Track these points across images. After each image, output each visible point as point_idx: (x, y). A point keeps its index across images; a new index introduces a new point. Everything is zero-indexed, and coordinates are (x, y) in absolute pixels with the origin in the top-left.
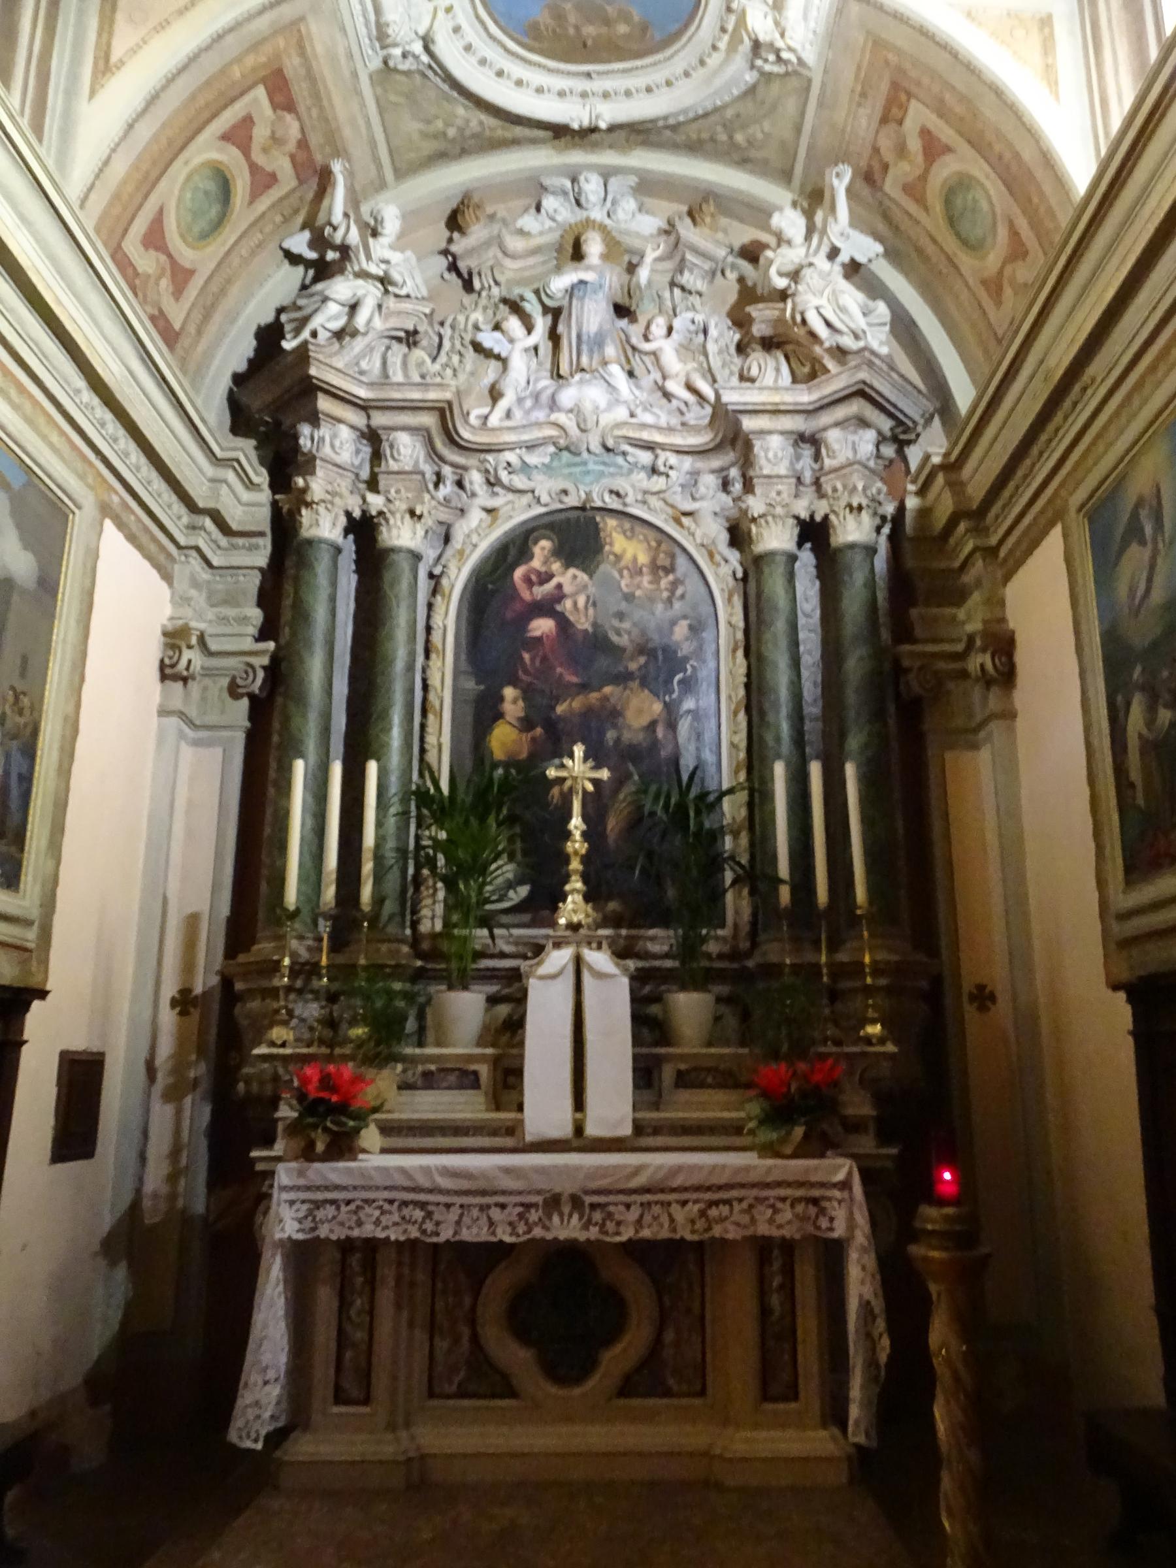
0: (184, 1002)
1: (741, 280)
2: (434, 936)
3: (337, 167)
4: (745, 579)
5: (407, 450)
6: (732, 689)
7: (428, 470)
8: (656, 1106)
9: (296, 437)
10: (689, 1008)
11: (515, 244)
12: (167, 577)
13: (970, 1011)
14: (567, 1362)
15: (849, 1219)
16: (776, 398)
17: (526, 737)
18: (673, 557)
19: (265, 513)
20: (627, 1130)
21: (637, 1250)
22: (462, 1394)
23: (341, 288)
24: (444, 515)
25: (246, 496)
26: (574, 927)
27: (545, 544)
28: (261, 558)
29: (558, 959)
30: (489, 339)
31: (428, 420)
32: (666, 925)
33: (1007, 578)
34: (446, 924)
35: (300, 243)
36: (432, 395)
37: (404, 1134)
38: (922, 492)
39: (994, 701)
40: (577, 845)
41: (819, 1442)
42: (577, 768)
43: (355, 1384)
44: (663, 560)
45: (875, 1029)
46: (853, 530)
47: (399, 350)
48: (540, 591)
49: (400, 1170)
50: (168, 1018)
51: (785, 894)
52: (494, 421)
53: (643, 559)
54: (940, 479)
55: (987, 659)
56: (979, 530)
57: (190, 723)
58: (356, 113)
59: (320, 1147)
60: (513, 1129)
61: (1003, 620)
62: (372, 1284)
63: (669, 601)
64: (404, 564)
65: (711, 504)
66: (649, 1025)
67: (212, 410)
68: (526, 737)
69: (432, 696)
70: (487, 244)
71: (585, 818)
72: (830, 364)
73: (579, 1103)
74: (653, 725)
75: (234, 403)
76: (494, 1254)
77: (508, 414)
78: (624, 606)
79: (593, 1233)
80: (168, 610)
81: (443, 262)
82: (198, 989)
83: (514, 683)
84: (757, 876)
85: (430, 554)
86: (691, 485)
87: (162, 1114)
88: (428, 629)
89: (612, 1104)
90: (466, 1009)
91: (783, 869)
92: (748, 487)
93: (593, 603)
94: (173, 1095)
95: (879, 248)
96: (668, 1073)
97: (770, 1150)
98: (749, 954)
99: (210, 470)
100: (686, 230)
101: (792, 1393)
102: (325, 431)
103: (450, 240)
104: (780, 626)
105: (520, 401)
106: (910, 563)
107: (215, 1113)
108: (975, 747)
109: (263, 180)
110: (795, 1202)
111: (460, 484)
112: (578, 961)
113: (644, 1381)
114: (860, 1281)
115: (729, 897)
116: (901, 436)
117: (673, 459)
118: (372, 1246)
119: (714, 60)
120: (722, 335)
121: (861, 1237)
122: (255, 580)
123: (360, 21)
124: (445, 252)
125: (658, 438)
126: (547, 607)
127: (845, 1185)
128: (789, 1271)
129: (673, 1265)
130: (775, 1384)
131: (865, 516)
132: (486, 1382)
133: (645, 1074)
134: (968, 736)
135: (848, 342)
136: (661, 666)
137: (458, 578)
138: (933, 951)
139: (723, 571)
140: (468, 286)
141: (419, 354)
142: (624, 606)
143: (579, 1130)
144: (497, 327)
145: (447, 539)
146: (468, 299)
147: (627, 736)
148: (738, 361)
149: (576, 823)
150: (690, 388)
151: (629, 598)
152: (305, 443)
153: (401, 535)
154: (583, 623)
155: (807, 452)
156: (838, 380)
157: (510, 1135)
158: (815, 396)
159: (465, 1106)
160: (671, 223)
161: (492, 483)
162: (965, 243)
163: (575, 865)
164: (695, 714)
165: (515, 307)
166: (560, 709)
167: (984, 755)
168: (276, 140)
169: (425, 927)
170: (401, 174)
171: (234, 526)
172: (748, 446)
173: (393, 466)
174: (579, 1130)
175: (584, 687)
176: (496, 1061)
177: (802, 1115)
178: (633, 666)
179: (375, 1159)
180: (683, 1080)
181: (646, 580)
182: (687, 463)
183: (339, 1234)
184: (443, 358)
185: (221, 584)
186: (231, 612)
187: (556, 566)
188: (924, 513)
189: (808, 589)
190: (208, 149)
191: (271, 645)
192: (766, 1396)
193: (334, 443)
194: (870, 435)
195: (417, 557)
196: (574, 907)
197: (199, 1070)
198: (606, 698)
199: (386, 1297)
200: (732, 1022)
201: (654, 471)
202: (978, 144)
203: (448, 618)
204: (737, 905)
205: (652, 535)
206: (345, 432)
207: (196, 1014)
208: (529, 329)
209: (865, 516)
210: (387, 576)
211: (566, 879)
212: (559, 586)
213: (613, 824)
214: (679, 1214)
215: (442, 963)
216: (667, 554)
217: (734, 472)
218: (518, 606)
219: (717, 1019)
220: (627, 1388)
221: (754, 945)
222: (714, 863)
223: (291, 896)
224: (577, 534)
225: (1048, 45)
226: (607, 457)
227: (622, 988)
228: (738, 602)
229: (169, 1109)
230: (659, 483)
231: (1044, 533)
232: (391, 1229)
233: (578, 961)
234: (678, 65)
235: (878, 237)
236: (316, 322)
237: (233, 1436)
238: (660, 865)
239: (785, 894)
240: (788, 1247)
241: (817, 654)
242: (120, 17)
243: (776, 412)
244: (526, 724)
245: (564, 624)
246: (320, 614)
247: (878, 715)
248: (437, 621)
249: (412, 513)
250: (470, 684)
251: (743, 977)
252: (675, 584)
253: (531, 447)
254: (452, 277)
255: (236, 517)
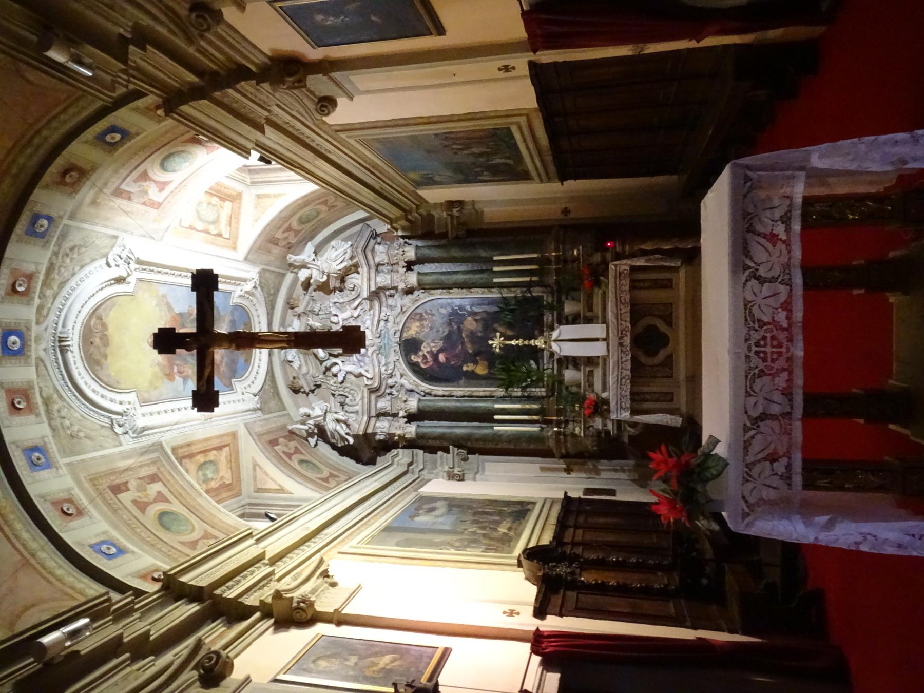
0: (568, 470)
1: (315, 290)
2: (546, 391)
3: (290, 427)
4: (424, 289)
5: (383, 404)
6: (464, 293)
7: (388, 398)
8: (598, 318)
9: (380, 441)
10: (569, 308)
11: (304, 370)
12: (430, 480)
13: (571, 216)
14: (664, 340)
15: (624, 265)
16: (365, 279)
17: (480, 362)
18: (417, 314)
19: (406, 451)
20: (604, 326)
21: (634, 322)
22: (672, 369)
23: (330, 426)
24: (403, 391)
25: (400, 457)
26: (545, 343)
27: (412, 358)
28: (421, 452)
29: (555, 347)
30: (340, 378)
31: (373, 396)
32: (543, 315)
33: (426, 202)
34: (543, 387)
35: (312, 441)
36: (366, 395)
37: (605, 388)
38: (397, 230)
39: (469, 207)
40: (520, 342)
41: (682, 274)
42: (496, 343)
43: (668, 397)
44: (418, 317)
45: (575, 252)
46: (411, 254)
47: (346, 408)
48: (429, 358)
49: (613, 387)
50: (573, 475)
51: (534, 279)
52: (369, 376)
53: (418, 324)
54: (394, 225)
55: (455, 210)
56: (410, 212)
57: (477, 472)
58: (274, 421)
59: (605, 407)
60: (605, 359)
61: (441, 204)
62: (643, 393)
63: (433, 315)
64: (422, 404)
65: (399, 301)
66: (575, 320)
67: (370, 470)
68: (480, 362)
69: (467, 394)
70: (306, 379)
71: (512, 340)
72: (354, 261)
73: (597, 340)
74: (476, 320)
75: (366, 463)
76: (634, 359)
77: (367, 371)
78: (434, 330)
79: (629, 334)
80: (441, 480)
81: (311, 395)
82: (564, 466)
83: (462, 367)
84: (529, 286)
85: (417, 396)
86: (391, 308)
87: (604, 475)
88: (443, 396)
89: (597, 330)
90: (569, 375)
91: (528, 279)
92: (396, 288)
93: (433, 341)
94: (598, 472)
95: (309, 243)
96: (589, 314)
97: (607, 286)
98: (552, 288)
99: (395, 466)
100: (299, 310)
101: (671, 280)
102: (378, 431)
103: (304, 392)
104: (443, 278)
105: (361, 367)
106: (420, 232)
107: (603, 459)
108: (482, 212)
109: (297, 451)
110: (620, 280)
111: (392, 387)
112: (555, 341)
113: (669, 320)
114: (640, 262)
115: (534, 294)
116: (374, 235)
117: (383, 314)
118: (632, 393)
119: (255, 301)
120: (337, 297)
121: (629, 262)
122: (426, 454)
123: (249, 417)
124: (307, 394)
125: (376, 319)
126: (435, 357)
127: (616, 266)
128: (639, 281)
129: (637, 312)
130: (667, 285)
131: (406, 249)
132: (669, 362)
133: (589, 321)
134: (480, 214)
135: (348, 256)
136: (456, 317)
137: (425, 386)
138: (552, 227)
139: (422, 297)
140: (318, 386)
141: (348, 401)
142: (434, 330)
143: (604, 340)
144: (335, 375)
145: (412, 391)
146: (324, 386)
147: (480, 328)
148: (346, 291)
149: (513, 343)
150: (355, 309)
151: (431, 328)
152: (382, 437)
153: (413, 404)
154: (441, 344)
155: (381, 268)
156: (360, 258)
157: (605, 359)
158: (365, 266)
159: (598, 373)
160: (294, 316)
161: (391, 376)
162: (317, 217)
163: (526, 343)
164: (472, 306)
165: (328, 369)
166: (470, 351)
167: (485, 209)
168: (286, 446)
169: (544, 394)
170: (284, 409)
171: (410, 460)
172: (380, 288)
173: (389, 408)
174: (604, 340)
175: (463, 343)
176: (586, 365)
177: (598, 275)
178: (456, 327)
179: (611, 395)
180: (591, 309)
181: (425, 323)
182: (384, 309)
183: (629, 401)
184: (346, 394)
185: (429, 466)
186: (439, 461)
187: (421, 353)
188: (403, 229)
189: (427, 268)
190: (295, 463)
191: (451, 447)
192: (671, 287)
193: (382, 428)
194: (377, 247)
195: (420, 400)
196: (539, 343)
197: (590, 465)
198: (467, 336)
199: (646, 389)
200: (574, 293)
201: (386, 320)
202: (291, 216)
203: (439, 390)
204: (537, 292)
205: (409, 321)
206: (378, 424)
207: (572, 467)
208: (336, 364)
209: (406, 249)
210: (428, 409)
211: (530, 345)
212: (428, 352)
213: (509, 333)
214: (623, 311)
215: (559, 380)
216: (416, 316)
217: (388, 293)
218: (435, 366)
219: (573, 299)
220: (670, 324)
221: (549, 286)
222: (525, 299)
223: (535, 429)
224: (410, 346)
225: (268, 196)
226: (382, 337)
227: (564, 328)
228: (432, 292)
229: (602, 473)
230: (391, 319)
231: (418, 194)
232: (628, 388)
233: (555, 341)
234: (254, 313)
235: (306, 244)
236: (343, 433)
237: (679, 426)
238: (525, 316)
239: (534, 279)
240: (633, 282)
241: (451, 265)
242: (264, 487)
243: (369, 279)
244: (476, 363)
245: (440, 351)
246: (440, 430)
247: (473, 246)
248: (440, 393)
249: (405, 401)
250: (462, 382)
251: (559, 291)
252: (426, 312)
253: (379, 363)
254: (316, 392)
255: (407, 460)
